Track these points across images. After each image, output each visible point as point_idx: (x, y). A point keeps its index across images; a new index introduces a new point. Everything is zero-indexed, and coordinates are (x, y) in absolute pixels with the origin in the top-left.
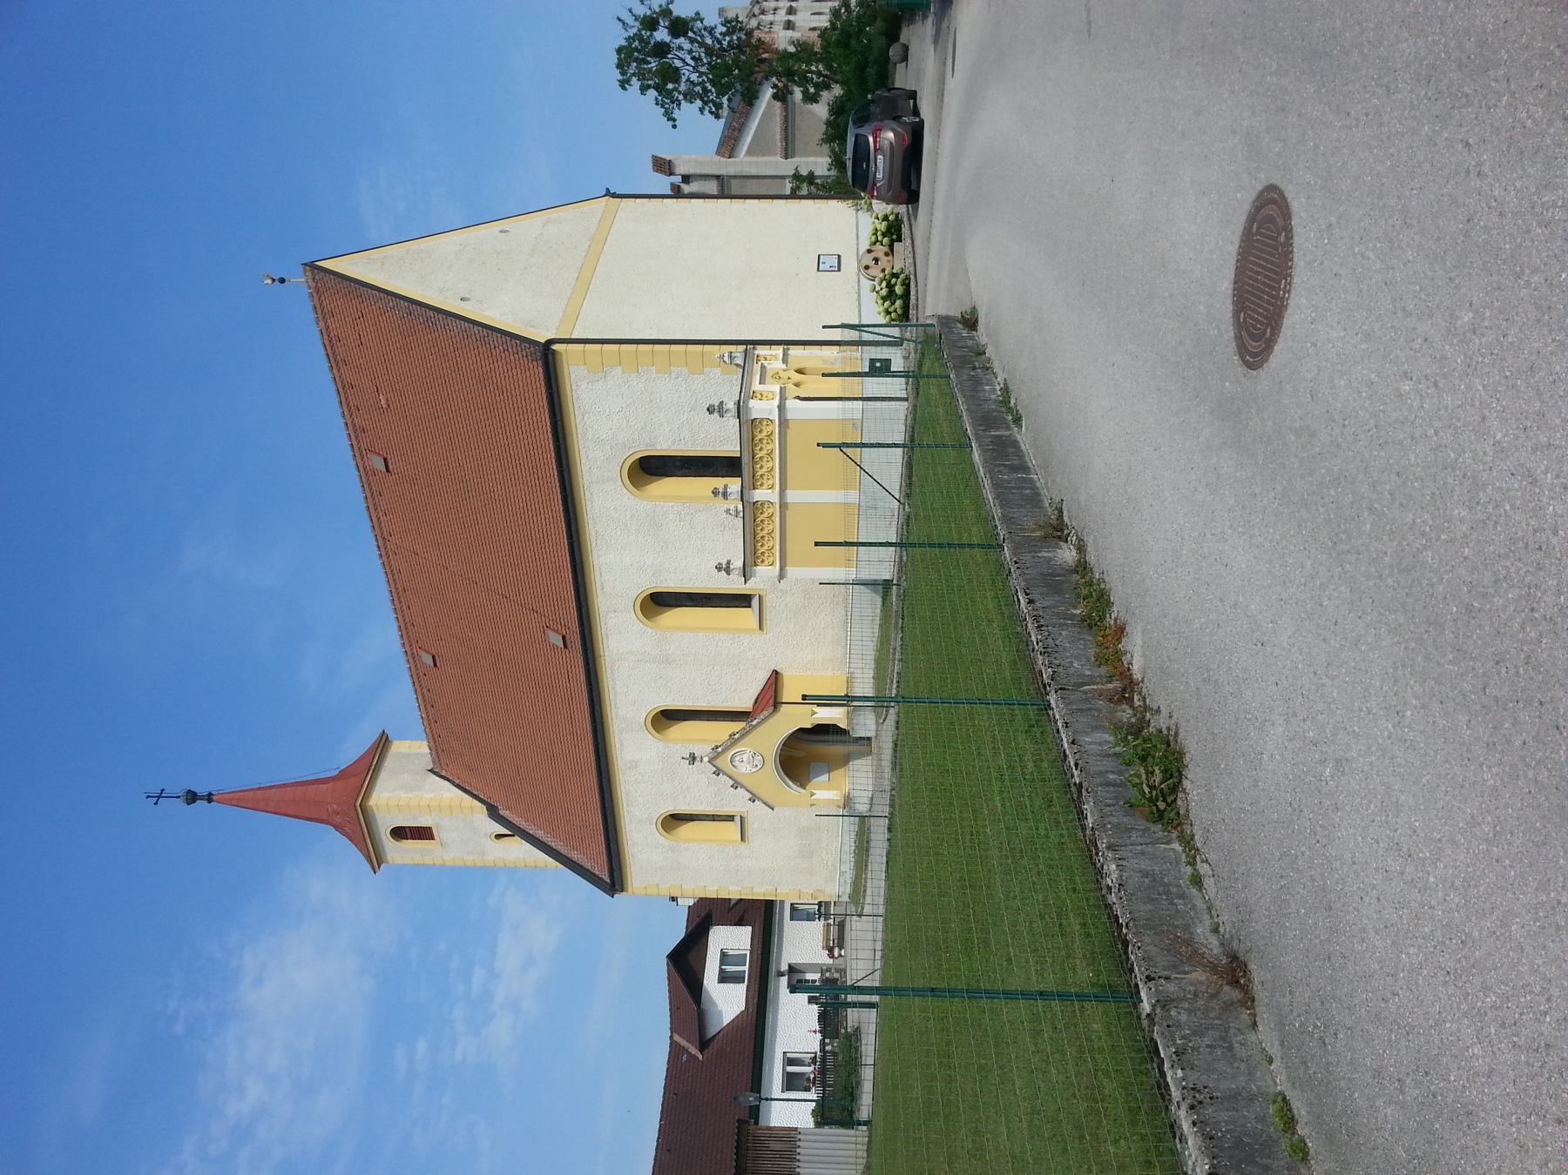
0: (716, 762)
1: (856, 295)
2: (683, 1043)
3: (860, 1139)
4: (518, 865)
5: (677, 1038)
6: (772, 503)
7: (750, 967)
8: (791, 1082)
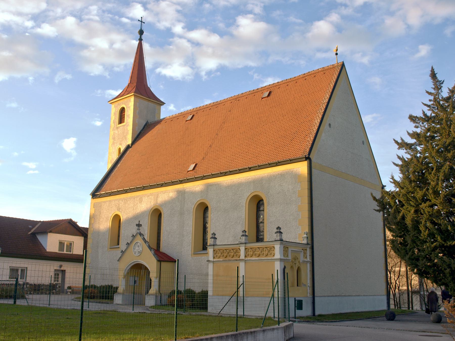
0: (139, 236)
1: (339, 295)
2: (37, 226)
3: (218, 298)
4: (436, 75)
5: (40, 224)
6: (274, 256)
7: (65, 254)
8: (14, 271)
